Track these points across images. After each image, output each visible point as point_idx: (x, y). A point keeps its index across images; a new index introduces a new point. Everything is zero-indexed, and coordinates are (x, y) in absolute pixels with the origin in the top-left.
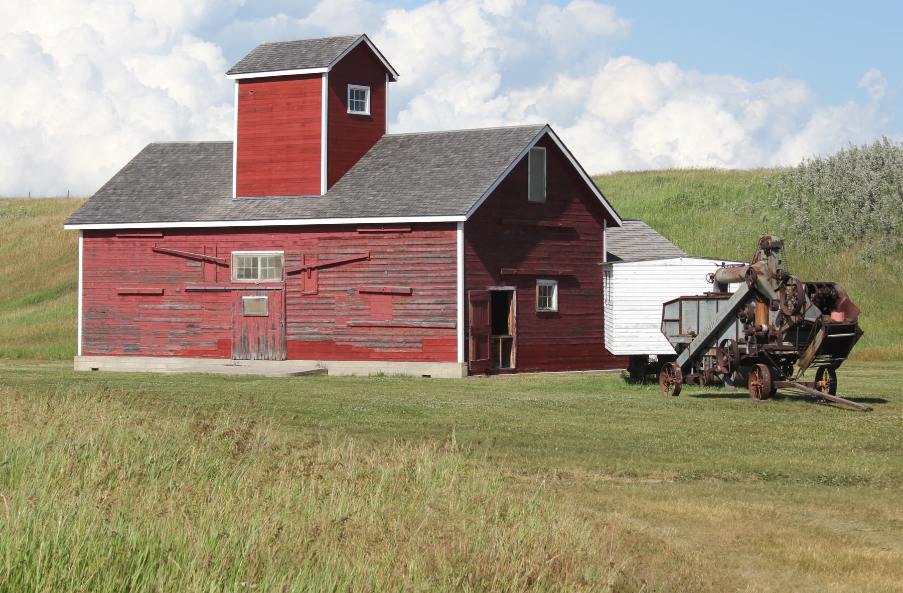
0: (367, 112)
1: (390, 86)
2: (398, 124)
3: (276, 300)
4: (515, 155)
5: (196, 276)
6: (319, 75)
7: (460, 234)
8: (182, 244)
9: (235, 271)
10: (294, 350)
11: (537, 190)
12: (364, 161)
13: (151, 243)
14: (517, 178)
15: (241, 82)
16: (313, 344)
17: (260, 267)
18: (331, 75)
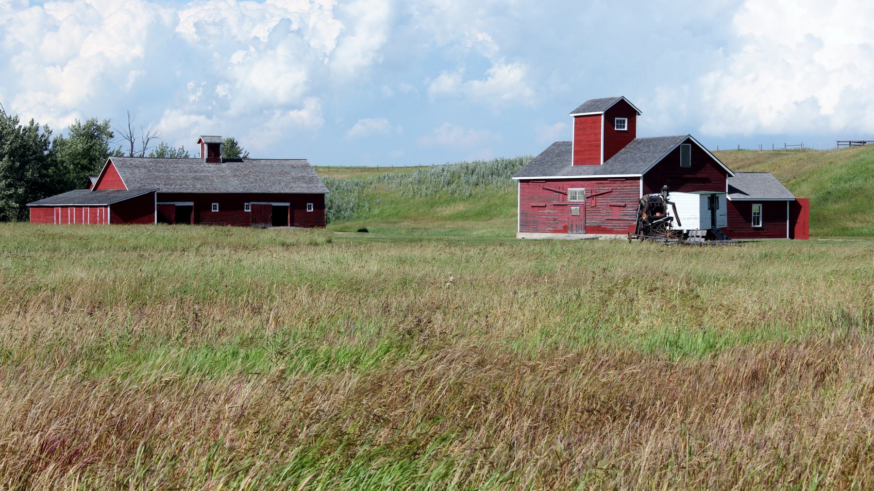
0: (626, 129)
1: (638, 117)
2: (640, 134)
3: (583, 208)
4: (673, 147)
5: (556, 199)
6: (600, 115)
7: (641, 182)
8: (551, 186)
9: (569, 197)
10: (589, 230)
11: (685, 161)
12: (623, 150)
13: (542, 185)
14: (674, 156)
15: (576, 117)
16: (594, 227)
17: (576, 194)
18: (606, 114)
